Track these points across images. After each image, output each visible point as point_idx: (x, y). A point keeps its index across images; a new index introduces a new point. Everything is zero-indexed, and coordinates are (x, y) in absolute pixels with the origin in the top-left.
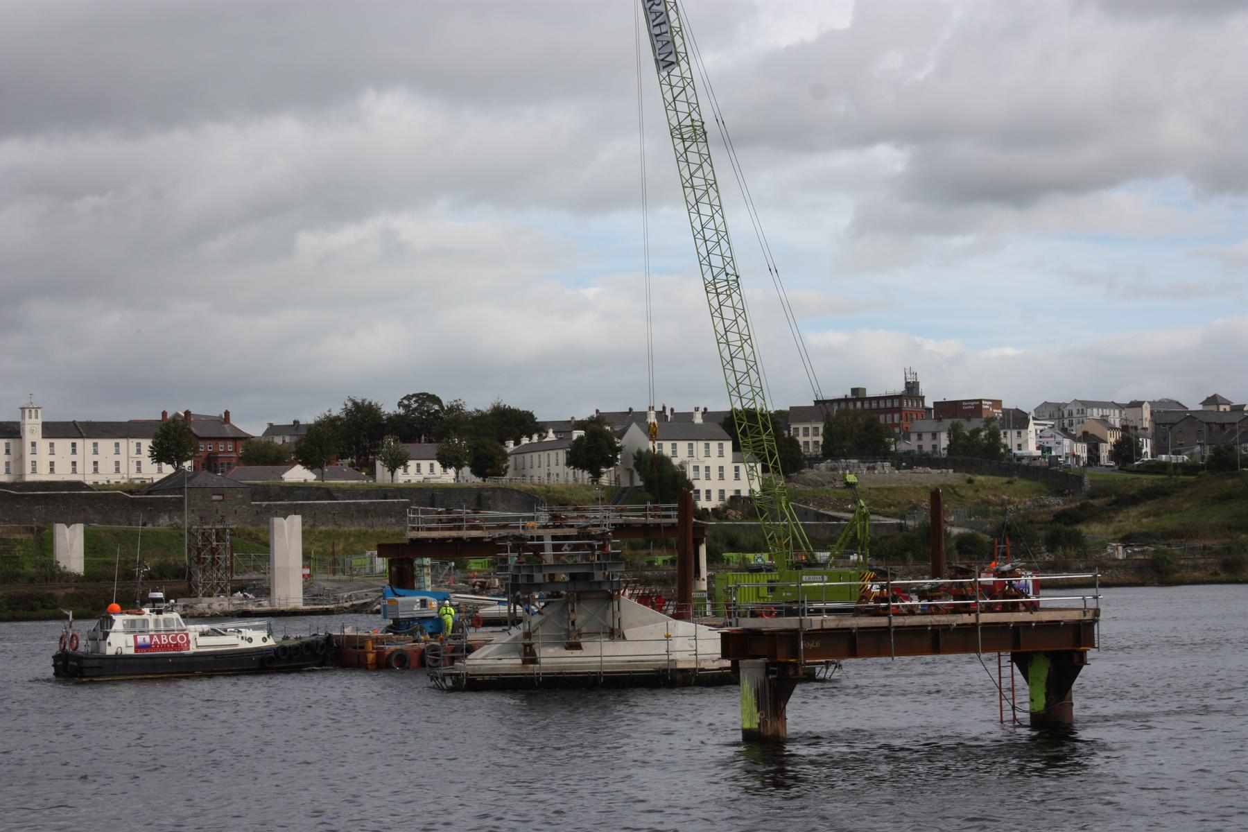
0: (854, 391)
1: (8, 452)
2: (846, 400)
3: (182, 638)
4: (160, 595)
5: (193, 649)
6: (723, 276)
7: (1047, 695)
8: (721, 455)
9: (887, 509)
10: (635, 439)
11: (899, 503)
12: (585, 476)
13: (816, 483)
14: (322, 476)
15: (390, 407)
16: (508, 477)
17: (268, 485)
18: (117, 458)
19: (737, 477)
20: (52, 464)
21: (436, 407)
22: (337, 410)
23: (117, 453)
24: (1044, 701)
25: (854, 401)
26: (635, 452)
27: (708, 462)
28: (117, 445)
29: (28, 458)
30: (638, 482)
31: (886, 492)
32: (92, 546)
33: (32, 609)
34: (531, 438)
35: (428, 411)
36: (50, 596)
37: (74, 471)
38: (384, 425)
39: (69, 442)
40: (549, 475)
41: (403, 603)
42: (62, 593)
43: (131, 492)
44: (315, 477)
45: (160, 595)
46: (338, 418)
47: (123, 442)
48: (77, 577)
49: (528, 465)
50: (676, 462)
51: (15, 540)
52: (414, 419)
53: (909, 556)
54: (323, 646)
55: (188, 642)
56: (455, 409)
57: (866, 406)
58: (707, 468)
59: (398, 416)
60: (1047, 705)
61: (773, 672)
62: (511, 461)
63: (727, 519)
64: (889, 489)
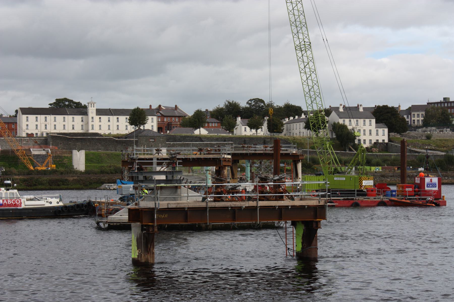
0: (445, 99)
1: (82, 121)
2: (441, 103)
3: (18, 201)
4: (9, 182)
5: (23, 206)
6: (303, 43)
7: (302, 243)
8: (370, 125)
9: (442, 149)
10: (334, 118)
11: (448, 146)
12: (312, 134)
13: (414, 137)
14: (210, 132)
15: (243, 104)
16: (284, 133)
17: (175, 135)
19: (377, 134)
20: (55, 125)
21: (262, 104)
22: (222, 105)
24: (301, 246)
25: (444, 103)
26: (332, 123)
27: (365, 128)
29: (90, 124)
30: (334, 136)
31: (444, 141)
32: (88, 159)
33: (58, 185)
34: (294, 117)
35: (259, 106)
36: (66, 180)
37: (64, 128)
38: (241, 112)
40: (300, 132)
41: (124, 187)
42: (71, 179)
43: (119, 138)
44: (207, 132)
45: (9, 182)
46: (222, 109)
48: (81, 173)
49: (292, 128)
50: (350, 128)
51: (65, 157)
52: (253, 109)
53: (439, 169)
54: (86, 206)
55: (21, 203)
56: (270, 105)
57: (449, 105)
58: (364, 130)
59: (246, 108)
60: (302, 248)
61: (145, 230)
62: (285, 127)
63: (372, 152)
64: (445, 140)
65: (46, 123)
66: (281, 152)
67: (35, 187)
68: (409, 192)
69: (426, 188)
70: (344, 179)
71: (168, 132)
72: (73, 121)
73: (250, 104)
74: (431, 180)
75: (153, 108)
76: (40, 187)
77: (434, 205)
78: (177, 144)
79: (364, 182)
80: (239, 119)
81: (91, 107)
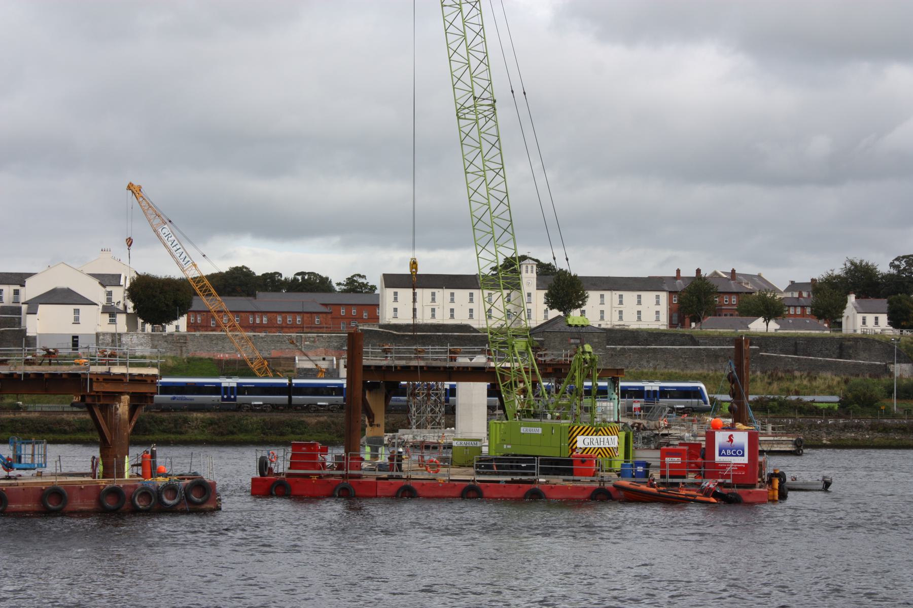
15: (884, 268)
18: (602, 307)
20: (452, 310)
23: (602, 303)
28: (602, 296)
33: (282, 434)
36: (302, 423)
39: (635, 294)
46: (838, 277)
47: (607, 294)
65: (622, 307)
66: (365, 362)
67: (230, 437)
68: (672, 466)
69: (718, 459)
70: (540, 431)
71: (693, 325)
72: (452, 301)
73: (898, 267)
74: (731, 439)
75: (703, 273)
76: (242, 437)
77: (713, 500)
78: (630, 349)
79: (580, 439)
80: (852, 298)
81: (527, 272)
